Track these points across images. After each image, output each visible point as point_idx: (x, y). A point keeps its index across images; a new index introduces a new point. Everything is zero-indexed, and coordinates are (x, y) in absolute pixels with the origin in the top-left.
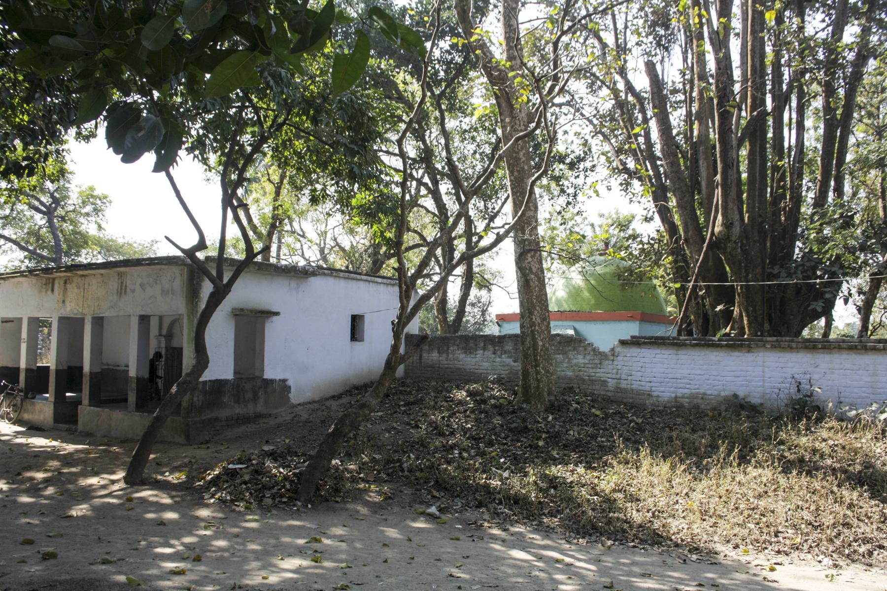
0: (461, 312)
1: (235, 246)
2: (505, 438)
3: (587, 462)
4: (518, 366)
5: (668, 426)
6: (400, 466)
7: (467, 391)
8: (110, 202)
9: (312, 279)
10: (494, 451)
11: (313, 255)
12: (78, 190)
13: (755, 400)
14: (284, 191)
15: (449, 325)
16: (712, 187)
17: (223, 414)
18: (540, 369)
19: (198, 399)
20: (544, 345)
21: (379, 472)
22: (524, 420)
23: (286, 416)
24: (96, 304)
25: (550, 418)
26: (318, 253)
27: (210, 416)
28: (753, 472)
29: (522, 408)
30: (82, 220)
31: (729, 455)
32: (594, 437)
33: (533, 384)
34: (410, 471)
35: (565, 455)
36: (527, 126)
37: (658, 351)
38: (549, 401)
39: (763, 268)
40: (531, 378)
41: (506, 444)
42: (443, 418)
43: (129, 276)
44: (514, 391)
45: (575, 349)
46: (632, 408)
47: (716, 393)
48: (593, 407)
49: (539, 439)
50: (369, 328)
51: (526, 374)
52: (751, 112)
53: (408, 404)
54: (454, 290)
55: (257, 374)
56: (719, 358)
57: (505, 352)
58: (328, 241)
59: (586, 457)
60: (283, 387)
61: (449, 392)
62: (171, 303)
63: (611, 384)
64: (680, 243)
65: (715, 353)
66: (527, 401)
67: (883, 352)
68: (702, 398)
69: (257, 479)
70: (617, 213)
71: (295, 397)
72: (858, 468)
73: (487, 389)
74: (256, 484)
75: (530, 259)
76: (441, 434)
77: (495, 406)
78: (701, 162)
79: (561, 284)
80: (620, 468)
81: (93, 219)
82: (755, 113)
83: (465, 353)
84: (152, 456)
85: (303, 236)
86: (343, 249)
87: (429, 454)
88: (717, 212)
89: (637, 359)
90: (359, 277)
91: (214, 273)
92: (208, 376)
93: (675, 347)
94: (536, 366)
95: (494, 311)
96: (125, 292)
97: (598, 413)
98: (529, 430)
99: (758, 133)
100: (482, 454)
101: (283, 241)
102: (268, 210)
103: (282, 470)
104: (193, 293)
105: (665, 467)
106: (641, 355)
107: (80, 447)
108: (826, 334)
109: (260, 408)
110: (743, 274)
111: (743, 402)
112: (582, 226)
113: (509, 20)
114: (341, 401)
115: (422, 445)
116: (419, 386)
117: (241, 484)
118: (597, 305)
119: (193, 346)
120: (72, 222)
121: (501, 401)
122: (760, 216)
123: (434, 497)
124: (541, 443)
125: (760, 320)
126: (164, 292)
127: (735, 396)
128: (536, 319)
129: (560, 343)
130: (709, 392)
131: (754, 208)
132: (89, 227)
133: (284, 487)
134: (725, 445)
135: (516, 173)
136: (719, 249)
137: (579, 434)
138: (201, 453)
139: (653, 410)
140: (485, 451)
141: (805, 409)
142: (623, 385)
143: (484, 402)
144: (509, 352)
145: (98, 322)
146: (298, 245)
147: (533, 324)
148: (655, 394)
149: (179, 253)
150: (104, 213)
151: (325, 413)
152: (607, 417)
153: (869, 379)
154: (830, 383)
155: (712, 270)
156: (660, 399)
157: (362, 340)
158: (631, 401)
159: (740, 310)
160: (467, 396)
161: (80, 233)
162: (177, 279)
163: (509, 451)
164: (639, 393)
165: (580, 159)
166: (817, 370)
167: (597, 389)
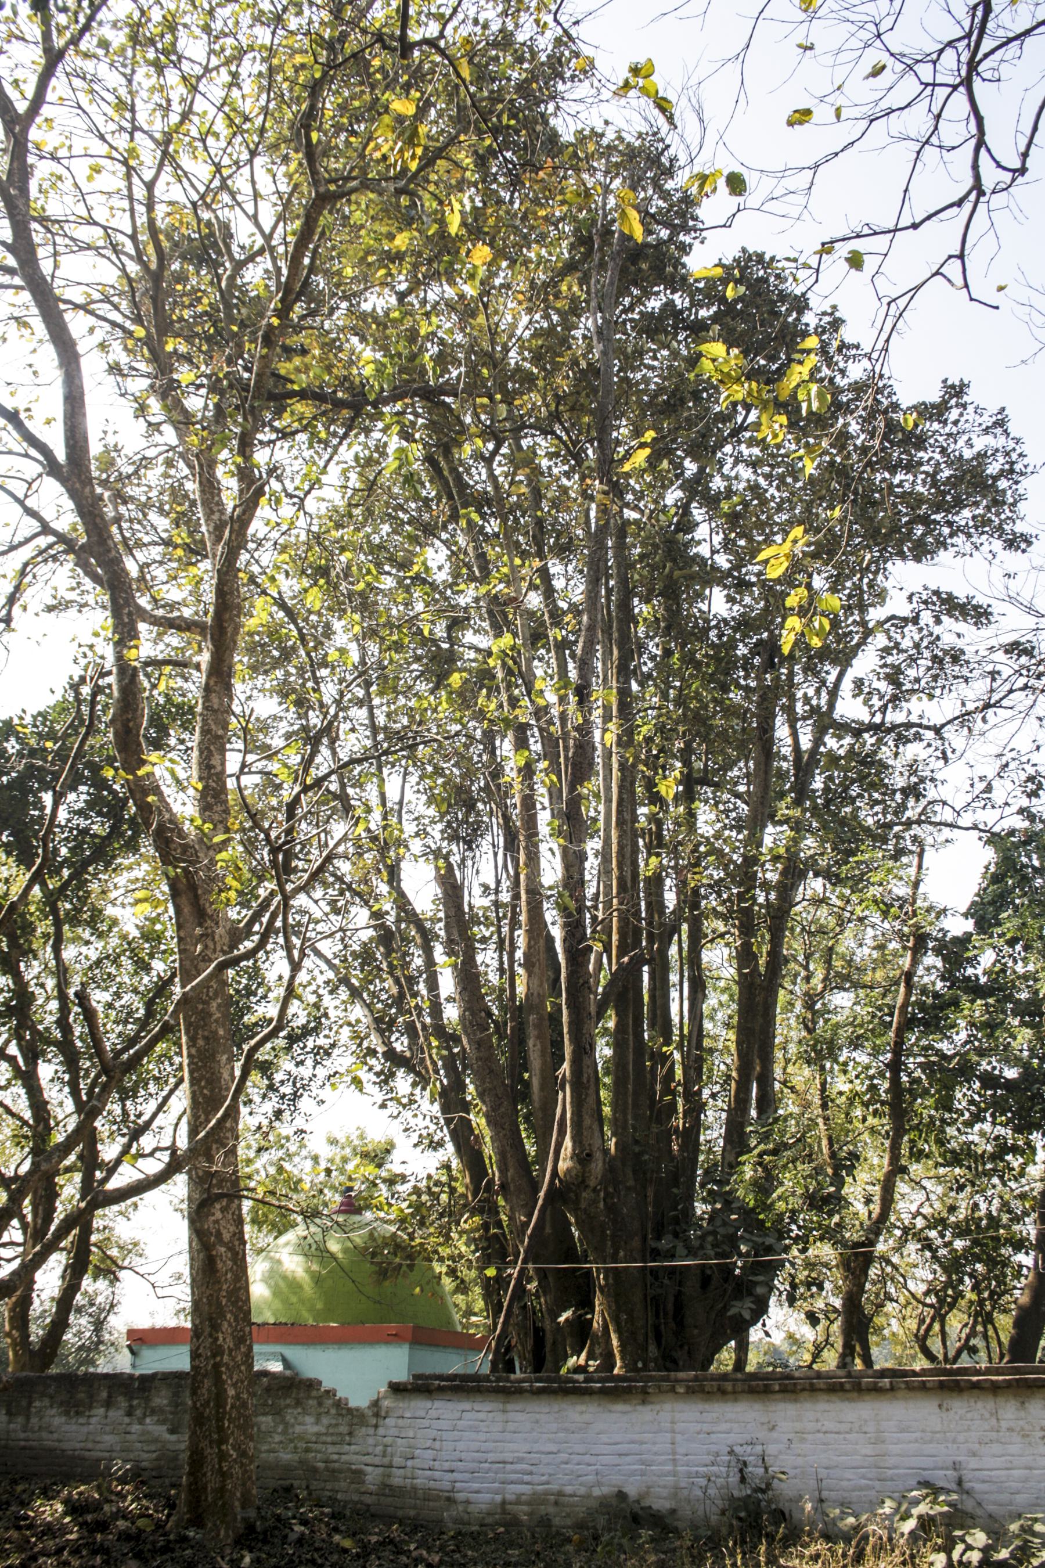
0: (60, 1324)
4: (180, 1442)
7: (66, 1502)
13: (660, 1504)
15: (32, 1353)
16: (551, 1085)
20: (237, 1397)
25: (247, 1560)
29: (184, 1539)
33: (212, 1481)
36: (234, 946)
37: (467, 1405)
38: (244, 1519)
39: (644, 1239)
40: (207, 1469)
45: (298, 1403)
47: (582, 1491)
48: (336, 1530)
51: (197, 1460)
52: (619, 957)
54: (49, 1280)
56: (587, 1417)
57: (153, 1412)
61: (25, 1504)
63: (373, 1476)
64: (489, 1184)
65: (580, 1408)
66: (197, 1522)
67: (889, 1395)
68: (556, 1503)
70: (362, 1137)
75: (218, 1215)
77: (125, 1536)
78: (531, 1043)
79: (275, 1265)
82: (626, 959)
83: (67, 1413)
88: (562, 1133)
89: (426, 1423)
95: (118, 1324)
97: (347, 1543)
99: (631, 994)
106: (433, 1413)
107: (53, 1228)
108: (740, 1363)
111: (636, 1508)
112: (296, 1159)
113: (210, 754)
118: (329, 1312)
121: (141, 1523)
125: (641, 1338)
127: (621, 1495)
128: (225, 1339)
129: (268, 1390)
130: (569, 1489)
131: (625, 1127)
135: (201, 1043)
136: (565, 1202)
139: (460, 1533)
143: (102, 1526)
144: (161, 1410)
148: (460, 1496)
152: (366, 1552)
153: (868, 1450)
154: (800, 1461)
155: (550, 1244)
156: (471, 1508)
158: (412, 1513)
160: (65, 1514)
164: (428, 1495)
165: (306, 1032)
166: (774, 1435)
167: (345, 1491)
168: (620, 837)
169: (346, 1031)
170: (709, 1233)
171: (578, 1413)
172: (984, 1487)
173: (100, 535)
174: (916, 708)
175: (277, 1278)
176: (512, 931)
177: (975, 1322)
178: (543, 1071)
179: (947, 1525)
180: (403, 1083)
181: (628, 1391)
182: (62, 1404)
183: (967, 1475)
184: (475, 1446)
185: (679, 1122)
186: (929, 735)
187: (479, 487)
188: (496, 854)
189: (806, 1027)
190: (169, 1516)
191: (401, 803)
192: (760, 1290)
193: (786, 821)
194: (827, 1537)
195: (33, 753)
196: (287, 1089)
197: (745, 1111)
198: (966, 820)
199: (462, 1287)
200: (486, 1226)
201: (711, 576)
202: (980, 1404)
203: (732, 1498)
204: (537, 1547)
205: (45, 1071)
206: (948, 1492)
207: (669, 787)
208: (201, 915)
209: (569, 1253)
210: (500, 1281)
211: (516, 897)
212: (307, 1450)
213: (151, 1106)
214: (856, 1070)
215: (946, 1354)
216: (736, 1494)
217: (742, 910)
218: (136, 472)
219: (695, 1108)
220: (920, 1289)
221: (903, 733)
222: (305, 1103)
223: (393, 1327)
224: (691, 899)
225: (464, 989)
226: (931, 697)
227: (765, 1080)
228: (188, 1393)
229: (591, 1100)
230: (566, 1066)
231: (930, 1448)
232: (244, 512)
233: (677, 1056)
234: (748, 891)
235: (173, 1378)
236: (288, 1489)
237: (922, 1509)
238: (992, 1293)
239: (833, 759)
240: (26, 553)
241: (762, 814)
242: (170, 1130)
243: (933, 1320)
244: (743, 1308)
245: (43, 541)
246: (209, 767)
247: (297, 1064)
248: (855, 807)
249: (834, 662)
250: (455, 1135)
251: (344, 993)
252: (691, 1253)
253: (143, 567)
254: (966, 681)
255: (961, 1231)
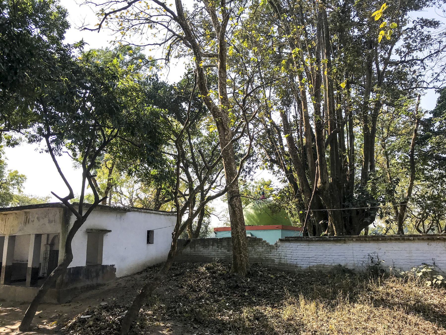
0: (199, 227)
1: (88, 199)
2: (227, 292)
3: (271, 304)
5: (309, 283)
6: (175, 310)
8: (26, 179)
9: (128, 213)
10: (222, 299)
11: (126, 203)
12: (9, 172)
13: (350, 267)
14: (113, 171)
17: (79, 285)
18: (242, 255)
19: (66, 278)
20: (243, 243)
21: (164, 315)
22: (236, 282)
23: (112, 284)
24: (12, 229)
25: (249, 280)
26: (129, 201)
27: (72, 287)
28: (358, 306)
29: (234, 275)
30: (10, 187)
31: (344, 298)
32: (272, 289)
33: (239, 262)
34: (180, 313)
35: (259, 300)
37: (299, 244)
39: (341, 203)
41: (228, 295)
42: (195, 282)
43: (31, 214)
44: (229, 266)
45: (257, 244)
46: (288, 273)
47: (330, 264)
48: (269, 273)
49: (245, 291)
50: (156, 237)
51: (235, 257)
52: (331, 131)
53: (176, 275)
55: (99, 263)
56: (330, 247)
57: (223, 247)
58: (134, 196)
59: (270, 301)
60: (112, 268)
61: (196, 268)
62: (52, 227)
63: (277, 261)
66: (236, 271)
67: (413, 241)
68: (323, 267)
69: (97, 324)
71: (118, 274)
72: (413, 303)
73: (215, 266)
74: (97, 327)
75: (235, 200)
76: (195, 291)
77: (220, 275)
80: (289, 307)
81: (16, 187)
83: (203, 247)
84: (37, 313)
85: (122, 194)
86: (141, 200)
87: (190, 303)
88: (318, 177)
89: (289, 248)
90: (151, 212)
91: (78, 211)
92: (72, 265)
93: (308, 242)
94: (240, 253)
96: (29, 222)
97: (272, 276)
98: (239, 287)
100: (217, 301)
101: (112, 196)
102: (105, 182)
103: (111, 317)
104: (65, 221)
105: (313, 305)
108: (366, 233)
109: (100, 281)
110: (332, 206)
112: (249, 187)
114: (142, 275)
115: (185, 298)
116: (181, 266)
117: (88, 328)
119: (64, 251)
120: (5, 188)
121: (223, 272)
122: (337, 178)
123: (194, 328)
124: (246, 294)
125: (341, 228)
126: (50, 222)
127: (340, 265)
129: (250, 241)
130: (326, 264)
131: (334, 175)
132: (14, 191)
133: (112, 327)
134: (341, 292)
135: (227, 160)
137: (265, 288)
138: (65, 309)
140: (218, 299)
141: (377, 272)
142: (283, 261)
143: (214, 272)
144: (225, 246)
145: (12, 238)
146: (119, 198)
147: (238, 232)
148: (299, 265)
149: (58, 201)
150: (23, 184)
151: (134, 282)
152: (277, 278)
153: (407, 255)
154: (388, 258)
157: (152, 243)
158: (287, 269)
159: (331, 223)
160: (206, 270)
161: (9, 194)
162: (57, 215)
163: (230, 299)
164: (291, 265)
166: (380, 251)
168: (329, 100)
169: (260, 156)
170: (358, 201)
171: (327, 246)
172: (442, 265)
173: (189, 34)
174: (416, 54)
175: (249, 216)
176: (301, 127)
177: (433, 222)
178: (311, 162)
179: (431, 274)
180: (276, 168)
181: (340, 240)
182: (202, 245)
183: (436, 262)
184: (302, 254)
185: (348, 173)
186: (419, 62)
187: (284, 8)
188: (295, 108)
189: (382, 146)
190: (229, 270)
191: (270, 96)
192: (372, 215)
193: (377, 92)
194: (396, 276)
195: (178, 93)
196: (247, 170)
197: (367, 169)
198: (431, 85)
199: (292, 216)
200: (299, 201)
201: (353, 24)
202: (440, 244)
203: (369, 266)
204: (319, 277)
205: (190, 170)
206: (431, 266)
207: (343, 85)
208: (224, 130)
209: (321, 207)
210: (304, 214)
211: (302, 118)
212: (261, 255)
213: (215, 176)
214: (399, 157)
215: (424, 231)
216: (371, 265)
217: (364, 116)
218: (193, 18)
219: (353, 169)
220: (416, 214)
221: (412, 62)
222: (252, 173)
223: (277, 226)
224: (350, 114)
225: (290, 142)
226: (421, 51)
227: (372, 161)
228: (231, 242)
229: (325, 169)
230: (318, 160)
231: (425, 255)
232: (225, 23)
233: (347, 157)
234: (366, 111)
235: (227, 239)
236: (257, 264)
237: (424, 270)
238: (438, 215)
239: (390, 72)
240: (170, 42)
241: (369, 89)
242: (219, 182)
243: (420, 222)
244: (368, 220)
245: (174, 38)
246: (223, 92)
247: (249, 164)
248: (398, 86)
249: (390, 44)
250: (289, 179)
251: (259, 146)
252: (354, 206)
253: (199, 42)
254: (431, 45)
255: (429, 198)
